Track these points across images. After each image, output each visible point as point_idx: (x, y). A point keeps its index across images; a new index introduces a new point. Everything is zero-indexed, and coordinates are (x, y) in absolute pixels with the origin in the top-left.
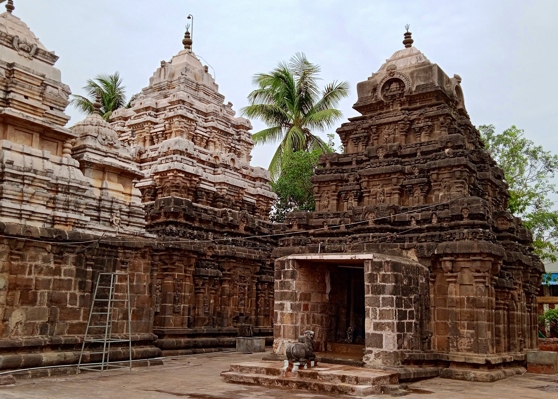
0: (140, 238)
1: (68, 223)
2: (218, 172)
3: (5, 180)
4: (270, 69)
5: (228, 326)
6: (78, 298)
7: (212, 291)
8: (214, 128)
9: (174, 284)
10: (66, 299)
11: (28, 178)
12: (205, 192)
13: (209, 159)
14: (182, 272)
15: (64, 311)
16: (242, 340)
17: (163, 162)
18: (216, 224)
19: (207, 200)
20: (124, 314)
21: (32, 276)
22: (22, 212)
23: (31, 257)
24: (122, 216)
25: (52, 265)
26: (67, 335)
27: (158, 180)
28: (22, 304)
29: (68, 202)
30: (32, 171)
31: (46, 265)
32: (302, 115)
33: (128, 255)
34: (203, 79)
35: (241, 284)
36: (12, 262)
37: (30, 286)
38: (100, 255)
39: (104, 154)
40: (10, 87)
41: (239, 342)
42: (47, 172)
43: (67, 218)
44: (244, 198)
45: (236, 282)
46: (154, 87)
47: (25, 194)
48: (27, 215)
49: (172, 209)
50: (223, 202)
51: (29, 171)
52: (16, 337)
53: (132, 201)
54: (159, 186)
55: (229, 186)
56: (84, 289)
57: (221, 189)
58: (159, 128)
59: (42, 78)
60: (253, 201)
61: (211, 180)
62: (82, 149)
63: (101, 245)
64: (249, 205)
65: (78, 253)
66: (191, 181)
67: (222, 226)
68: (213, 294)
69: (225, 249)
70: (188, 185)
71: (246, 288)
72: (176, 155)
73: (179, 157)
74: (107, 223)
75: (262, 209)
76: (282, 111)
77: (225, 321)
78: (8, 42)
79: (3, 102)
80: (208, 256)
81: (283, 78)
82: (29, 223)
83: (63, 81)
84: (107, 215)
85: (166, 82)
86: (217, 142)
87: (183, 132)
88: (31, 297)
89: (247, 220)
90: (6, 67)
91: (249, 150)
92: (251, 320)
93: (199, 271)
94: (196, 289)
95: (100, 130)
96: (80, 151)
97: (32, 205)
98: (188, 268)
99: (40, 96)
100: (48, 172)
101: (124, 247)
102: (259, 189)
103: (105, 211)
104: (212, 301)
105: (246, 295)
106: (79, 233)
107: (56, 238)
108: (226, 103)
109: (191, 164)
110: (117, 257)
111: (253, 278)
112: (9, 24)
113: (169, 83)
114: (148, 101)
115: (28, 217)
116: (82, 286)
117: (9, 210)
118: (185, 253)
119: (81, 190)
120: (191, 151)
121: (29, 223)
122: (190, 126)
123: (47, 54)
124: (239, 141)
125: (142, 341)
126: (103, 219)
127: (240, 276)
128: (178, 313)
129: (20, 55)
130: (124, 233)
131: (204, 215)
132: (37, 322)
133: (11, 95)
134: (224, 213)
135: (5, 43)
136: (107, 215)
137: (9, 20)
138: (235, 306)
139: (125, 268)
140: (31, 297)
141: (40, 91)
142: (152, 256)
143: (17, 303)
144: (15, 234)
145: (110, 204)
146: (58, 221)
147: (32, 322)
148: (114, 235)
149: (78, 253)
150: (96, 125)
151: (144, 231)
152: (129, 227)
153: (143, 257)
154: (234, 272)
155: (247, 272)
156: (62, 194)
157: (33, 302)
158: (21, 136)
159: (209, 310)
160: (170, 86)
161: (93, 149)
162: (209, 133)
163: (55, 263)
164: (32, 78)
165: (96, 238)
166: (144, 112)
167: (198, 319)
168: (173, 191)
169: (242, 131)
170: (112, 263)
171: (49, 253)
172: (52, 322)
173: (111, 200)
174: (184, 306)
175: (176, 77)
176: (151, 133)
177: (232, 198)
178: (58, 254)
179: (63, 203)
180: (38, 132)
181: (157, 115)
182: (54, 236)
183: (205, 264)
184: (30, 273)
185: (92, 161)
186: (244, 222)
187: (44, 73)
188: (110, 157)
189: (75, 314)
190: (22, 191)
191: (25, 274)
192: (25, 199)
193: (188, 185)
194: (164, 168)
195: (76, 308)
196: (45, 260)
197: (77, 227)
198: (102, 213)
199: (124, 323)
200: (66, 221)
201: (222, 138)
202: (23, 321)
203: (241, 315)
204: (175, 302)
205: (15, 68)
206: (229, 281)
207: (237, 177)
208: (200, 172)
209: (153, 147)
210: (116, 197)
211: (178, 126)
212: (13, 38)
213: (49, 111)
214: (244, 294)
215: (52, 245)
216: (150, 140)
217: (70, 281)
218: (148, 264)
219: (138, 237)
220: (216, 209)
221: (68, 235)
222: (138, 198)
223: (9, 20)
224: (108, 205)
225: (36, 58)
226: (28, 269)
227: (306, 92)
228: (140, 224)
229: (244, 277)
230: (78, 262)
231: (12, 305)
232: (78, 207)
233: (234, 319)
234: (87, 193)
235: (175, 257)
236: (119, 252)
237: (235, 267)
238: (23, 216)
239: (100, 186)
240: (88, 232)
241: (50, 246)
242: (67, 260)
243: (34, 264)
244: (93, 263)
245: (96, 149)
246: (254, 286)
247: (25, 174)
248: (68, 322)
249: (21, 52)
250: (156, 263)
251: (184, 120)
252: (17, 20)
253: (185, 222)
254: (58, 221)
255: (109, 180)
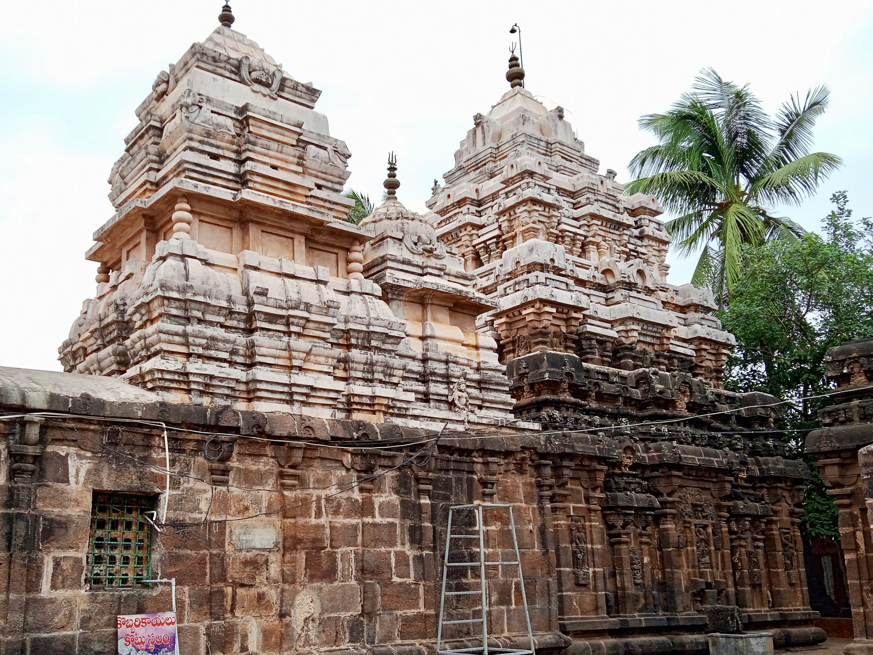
0: (508, 431)
1: (376, 408)
2: (616, 300)
3: (256, 329)
4: (666, 104)
5: (685, 610)
6: (411, 562)
7: (645, 539)
8: (593, 216)
9: (569, 526)
10: (389, 564)
11: (296, 321)
12: (598, 341)
13: (594, 276)
14: (581, 503)
15: (388, 590)
16: (723, 640)
17: (508, 291)
18: (629, 401)
19: (602, 356)
20: (500, 593)
21: (323, 520)
22: (294, 389)
23: (318, 481)
24: (469, 390)
25: (357, 495)
26: (399, 641)
27: (504, 327)
28: (312, 578)
29: (370, 365)
30: (302, 307)
31: (345, 495)
32: (743, 181)
33: (494, 468)
34: (556, 133)
35: (697, 521)
36: (286, 493)
37: (321, 540)
38: (441, 470)
39: (420, 271)
40: (245, 151)
41: (714, 644)
42: (328, 307)
43: (373, 397)
44: (672, 348)
45: (687, 519)
46: (465, 165)
47: (294, 354)
48: (303, 394)
49: (547, 375)
50: (634, 358)
51: (296, 308)
52: (307, 648)
53: (481, 359)
54: (507, 337)
55: (641, 324)
56: (420, 542)
57: (627, 331)
58: (489, 233)
59: (298, 130)
60: (689, 352)
61: (602, 316)
62: (377, 265)
63: (443, 448)
64: (682, 361)
65: (399, 469)
66: (567, 320)
67: (641, 405)
68: (647, 543)
69: (658, 450)
70: (564, 329)
71: (710, 530)
72: (533, 274)
73: (542, 276)
74: (443, 406)
75: (707, 368)
76: (706, 179)
77: (678, 599)
78: (232, 72)
79: (236, 182)
80: (625, 466)
81: (693, 118)
82: (307, 411)
83: (334, 134)
84: (441, 389)
85: (490, 150)
86: (603, 243)
87: (536, 230)
88: (325, 564)
89: (690, 388)
90: (234, 116)
91: (663, 253)
92: (727, 596)
93: (615, 499)
94: (611, 536)
95: (406, 226)
96: (376, 270)
97: (309, 374)
98: (592, 494)
99: (298, 164)
100: (329, 307)
101: (485, 452)
102: (697, 327)
103: (437, 382)
104: (646, 560)
105: (712, 543)
106: (397, 426)
107: (358, 438)
108: (602, 171)
109: (563, 286)
110: (472, 472)
111: (718, 507)
112: (230, 43)
113: (494, 151)
114: (462, 188)
115: (304, 398)
116: (416, 536)
117: (270, 387)
118: (585, 464)
119: (391, 341)
120: (560, 263)
121: (307, 411)
122: (549, 217)
123: (300, 88)
124: (641, 238)
125: (543, 649)
126: (436, 397)
127: (694, 506)
128: (585, 585)
129: (254, 92)
130: (478, 424)
131: (605, 385)
132: (343, 615)
133: (249, 166)
134: (642, 379)
135: (228, 74)
136: (441, 389)
137: (228, 37)
138: (693, 567)
139: (491, 495)
140: (325, 564)
141: (298, 154)
142: (538, 467)
143: (301, 576)
144: (285, 434)
145: (443, 366)
146: (357, 404)
147: (332, 615)
148: (460, 428)
149: (399, 469)
150: (397, 218)
151: (511, 417)
152: (483, 412)
153: (521, 471)
154: (680, 497)
155: (705, 496)
156: (358, 350)
157: (330, 574)
158: (273, 243)
159: (643, 578)
160: (497, 155)
161: (398, 261)
162: (586, 228)
163: (361, 490)
164: (280, 131)
165: (430, 434)
166: (457, 210)
167: (624, 597)
168: (537, 344)
169: (645, 219)
170: (465, 486)
171: (348, 470)
172: (368, 614)
173: (444, 358)
174: (594, 572)
175: (506, 137)
176: (474, 246)
177: (649, 349)
178: (365, 472)
179: (361, 367)
180: (300, 234)
181: (480, 212)
182: (355, 435)
183: (622, 482)
184: (319, 514)
185: (402, 284)
186: (684, 393)
187: (301, 120)
188: (431, 274)
189: (408, 594)
190: (288, 348)
191: (310, 517)
192: (296, 363)
193: (564, 329)
194: (514, 302)
195: (409, 585)
196: (343, 486)
197: (392, 415)
198: (431, 385)
199: (502, 612)
200: (372, 404)
201: (609, 235)
202: (316, 615)
203: (709, 585)
204: (576, 563)
205: (249, 113)
206: (674, 516)
207: (654, 306)
208: (584, 302)
209: (481, 270)
210: (453, 353)
211: (528, 220)
212: (240, 62)
213: (316, 192)
214: (707, 542)
215: (354, 454)
216: (473, 259)
217: (392, 525)
218: (531, 484)
219: (504, 430)
220: (625, 372)
221: (378, 431)
222: (491, 352)
223: (228, 37)
224: (440, 368)
225: (281, 97)
226: (314, 505)
227: (749, 133)
228: (504, 403)
229: (701, 506)
230: (402, 486)
231: (294, 582)
232: (391, 375)
233: (694, 595)
234: (401, 348)
235: (566, 472)
236: (474, 462)
237: (681, 487)
238: (296, 397)
239: (420, 334)
240: (413, 424)
241: (349, 456)
242: (381, 483)
243: (323, 493)
244: (430, 487)
245: (403, 263)
246: (723, 524)
247: (291, 312)
248: (399, 612)
249: (257, 87)
250: (548, 482)
251: (537, 208)
252: (241, 38)
253: (573, 399)
254: (357, 404)
255: (435, 320)
